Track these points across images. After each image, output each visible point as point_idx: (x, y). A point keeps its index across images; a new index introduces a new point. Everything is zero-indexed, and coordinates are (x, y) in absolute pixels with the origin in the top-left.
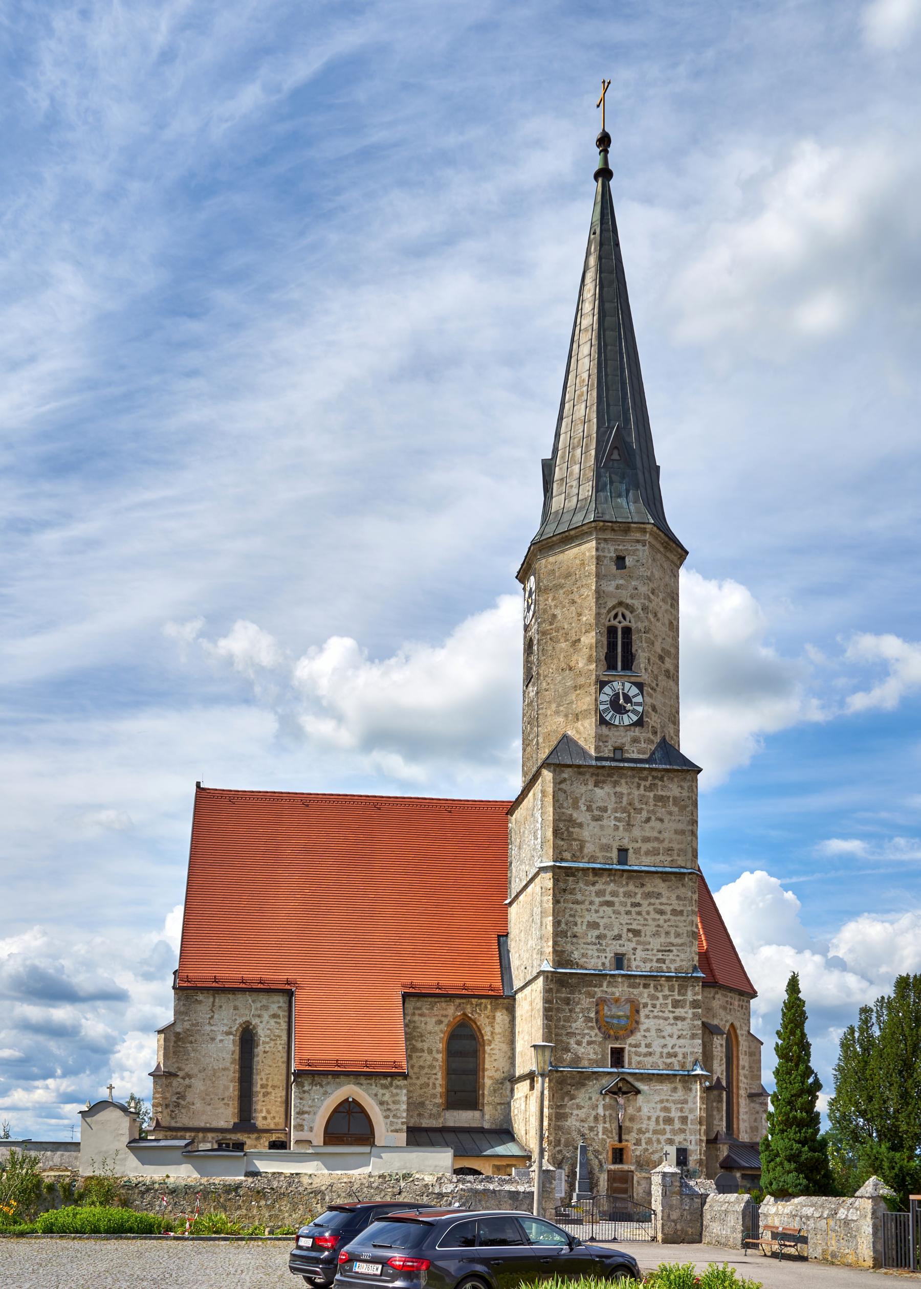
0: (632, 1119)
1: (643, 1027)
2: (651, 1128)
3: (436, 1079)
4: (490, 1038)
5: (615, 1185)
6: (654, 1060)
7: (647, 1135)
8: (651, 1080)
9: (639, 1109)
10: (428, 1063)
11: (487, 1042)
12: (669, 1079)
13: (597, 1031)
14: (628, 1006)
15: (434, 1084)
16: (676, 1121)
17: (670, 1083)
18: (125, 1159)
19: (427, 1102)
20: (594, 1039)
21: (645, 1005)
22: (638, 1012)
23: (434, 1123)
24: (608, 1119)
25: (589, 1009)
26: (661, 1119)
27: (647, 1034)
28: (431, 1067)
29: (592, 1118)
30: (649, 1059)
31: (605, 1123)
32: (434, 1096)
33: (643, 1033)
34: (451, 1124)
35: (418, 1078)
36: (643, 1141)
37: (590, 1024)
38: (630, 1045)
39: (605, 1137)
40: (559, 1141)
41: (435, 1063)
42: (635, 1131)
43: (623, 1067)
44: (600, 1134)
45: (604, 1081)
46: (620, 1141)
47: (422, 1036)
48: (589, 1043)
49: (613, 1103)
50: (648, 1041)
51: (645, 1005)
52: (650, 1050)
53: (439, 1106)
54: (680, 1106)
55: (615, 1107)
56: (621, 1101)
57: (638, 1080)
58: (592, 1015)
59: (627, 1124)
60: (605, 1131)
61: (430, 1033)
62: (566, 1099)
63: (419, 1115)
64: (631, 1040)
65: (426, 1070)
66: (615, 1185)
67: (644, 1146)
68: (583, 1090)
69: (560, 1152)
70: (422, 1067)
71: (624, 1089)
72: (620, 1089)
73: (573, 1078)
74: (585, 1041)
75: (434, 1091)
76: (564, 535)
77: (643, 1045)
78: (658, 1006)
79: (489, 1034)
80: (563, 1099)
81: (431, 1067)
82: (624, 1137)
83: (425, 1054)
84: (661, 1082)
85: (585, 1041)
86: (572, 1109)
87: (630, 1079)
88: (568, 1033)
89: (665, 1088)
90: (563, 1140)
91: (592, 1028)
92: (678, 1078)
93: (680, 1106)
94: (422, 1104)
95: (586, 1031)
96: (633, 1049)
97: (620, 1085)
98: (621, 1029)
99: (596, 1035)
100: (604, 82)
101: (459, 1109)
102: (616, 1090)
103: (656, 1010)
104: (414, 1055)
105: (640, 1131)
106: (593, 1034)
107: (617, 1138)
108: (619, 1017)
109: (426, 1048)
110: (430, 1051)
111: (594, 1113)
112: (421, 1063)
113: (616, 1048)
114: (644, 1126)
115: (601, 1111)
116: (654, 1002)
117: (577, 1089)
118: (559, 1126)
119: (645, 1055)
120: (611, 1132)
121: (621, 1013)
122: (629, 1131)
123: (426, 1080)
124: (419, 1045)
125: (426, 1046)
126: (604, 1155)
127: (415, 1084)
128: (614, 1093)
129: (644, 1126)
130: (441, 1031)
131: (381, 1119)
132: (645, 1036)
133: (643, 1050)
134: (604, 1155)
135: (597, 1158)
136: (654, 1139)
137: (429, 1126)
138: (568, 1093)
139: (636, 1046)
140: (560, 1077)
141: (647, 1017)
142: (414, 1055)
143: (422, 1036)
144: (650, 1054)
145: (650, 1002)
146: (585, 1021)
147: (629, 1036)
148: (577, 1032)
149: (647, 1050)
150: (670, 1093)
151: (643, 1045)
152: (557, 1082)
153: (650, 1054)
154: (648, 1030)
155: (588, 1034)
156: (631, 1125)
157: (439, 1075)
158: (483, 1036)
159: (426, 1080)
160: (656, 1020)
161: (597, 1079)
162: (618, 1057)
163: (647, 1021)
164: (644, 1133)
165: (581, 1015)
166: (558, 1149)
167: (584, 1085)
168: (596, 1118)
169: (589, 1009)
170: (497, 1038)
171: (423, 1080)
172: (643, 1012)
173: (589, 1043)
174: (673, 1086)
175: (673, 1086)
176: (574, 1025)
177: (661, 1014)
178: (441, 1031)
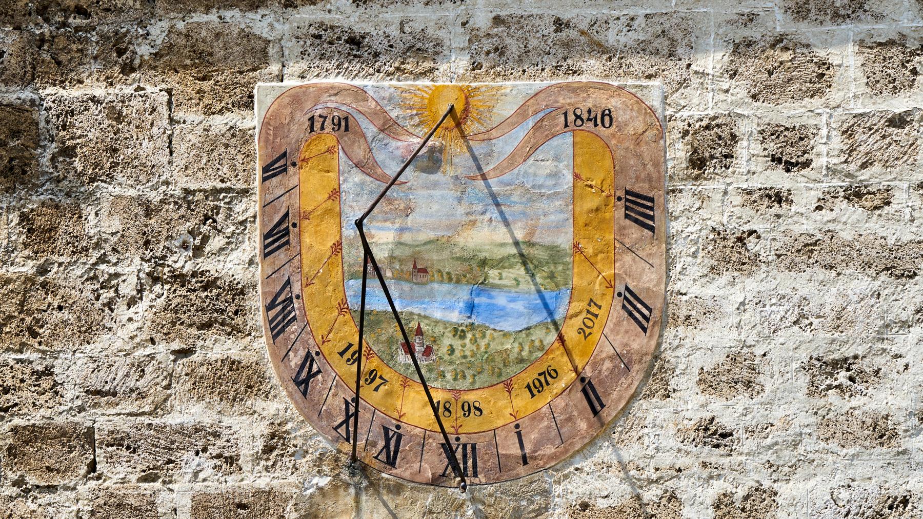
1: (694, 348)
13: (279, 404)
18: (392, 258)
21: (711, 150)
22: (641, 208)
25: (205, 211)
33: (691, 403)
37: (218, 348)
51: (711, 150)
58: (237, 261)
78: (826, 151)
88: (32, 435)
91: (236, 383)
95: (189, 412)
99: (275, 443)
100: (347, 129)
103: (804, 188)
106: (246, 430)
108: (475, 271)
116: (790, 112)
132: (715, 435)
141: (734, 251)
145: (752, 116)
146: (171, 320)
148: (105, 420)
154: (738, 374)
155: (202, 437)
160: (804, 284)
163: (730, 291)
165: (132, 269)
169: (205, 211)
172: (698, 212)
176: (74, 367)
177: (850, 220)
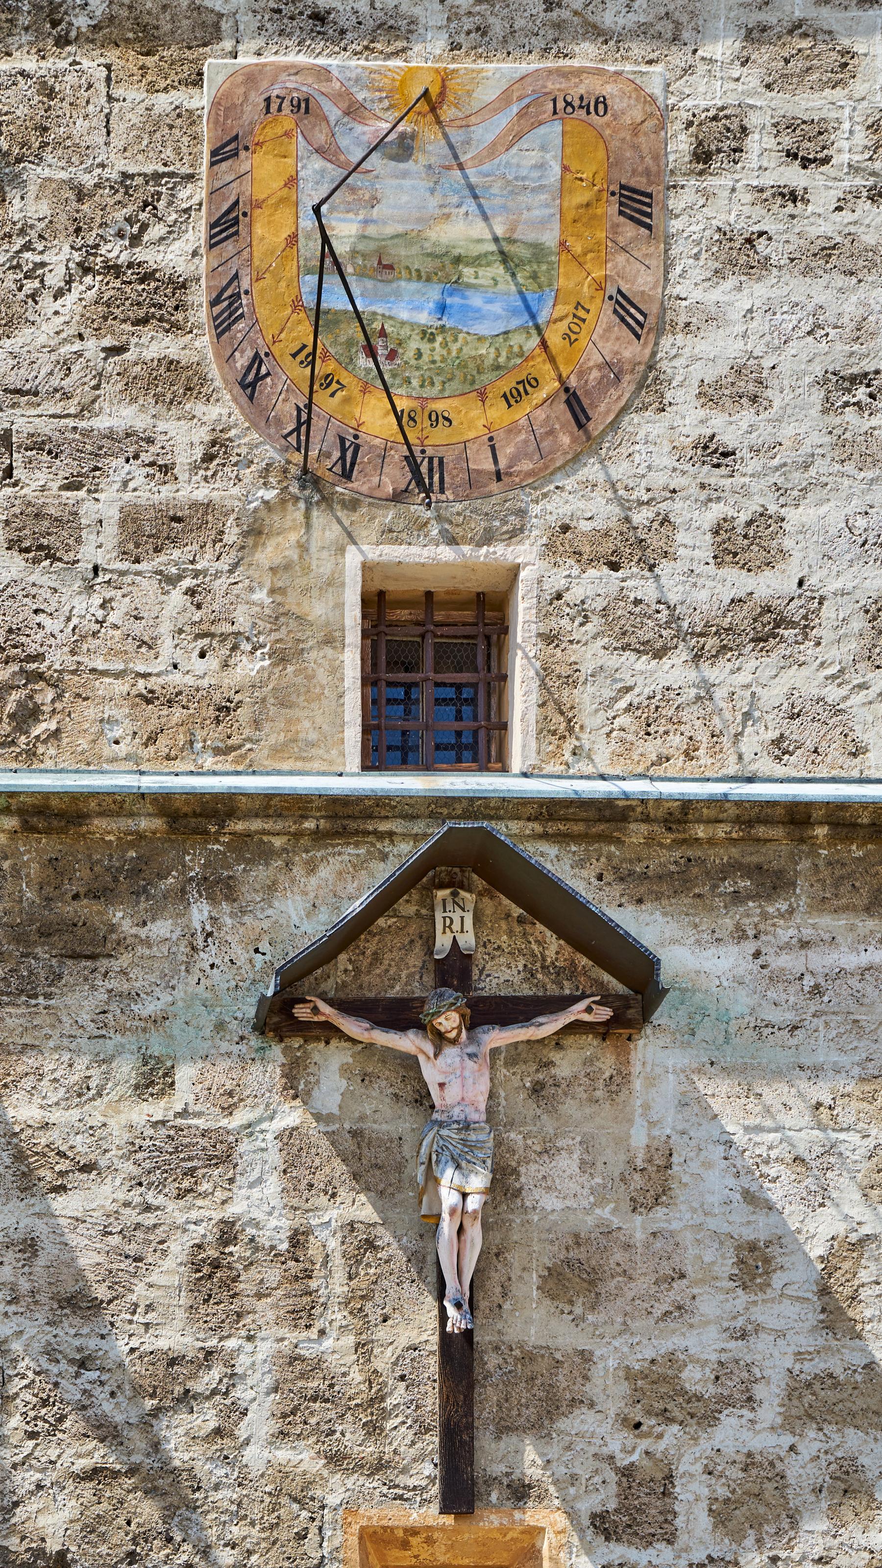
1: (693, 359)
6: (806, 681)
7: (731, 1434)
8: (773, 883)
9: (654, 1181)
13: (223, 409)
14: (542, 153)
20: (190, 490)
22: (637, 204)
25: (146, 197)
27: (732, 428)
29: (169, 1271)
30: (765, 679)
31: (303, 1314)
33: (689, 419)
36: (693, 1496)
37: (154, 345)
38: (562, 539)
43: (504, 770)
44: (258, 1423)
48: (150, 533)
49: (386, 1117)
50: (747, 494)
52: (770, 585)
56: (459, 1078)
57: (644, 886)
58: (179, 252)
59: (530, 1322)
60: (305, 1397)
64: (580, 500)
71: (500, 977)
74: (105, 505)
76: (299, 765)
77: (693, 543)
82: (492, 1455)
85: (105, 505)
87: (568, 868)
91: (175, 384)
95: (118, 415)
96: (592, 584)
98: (473, 381)
99: (215, 451)
103: (822, 187)
105: (659, 1395)
106: (183, 435)
108: (447, 269)
111: (190, 1222)
113: (484, 768)
114: (701, 1344)
116: (809, 103)
119: (716, 640)
120: (374, 1414)
121: (463, 231)
122: (549, 1403)
133: (694, 583)
136: (801, 1471)
139: (631, 547)
141: (741, 254)
144: (769, 627)
145: (765, 109)
147: (546, 472)
149: (734, 582)
151: (693, 543)
153: (769, 627)
154: (744, 387)
155: (133, 443)
160: (821, 291)
161: (219, 887)
162: (435, 664)
163: (737, 297)
165: (60, 258)
167: (89, 948)
168: (213, 1273)
169: (146, 197)
172: (699, 211)
173: (150, 533)
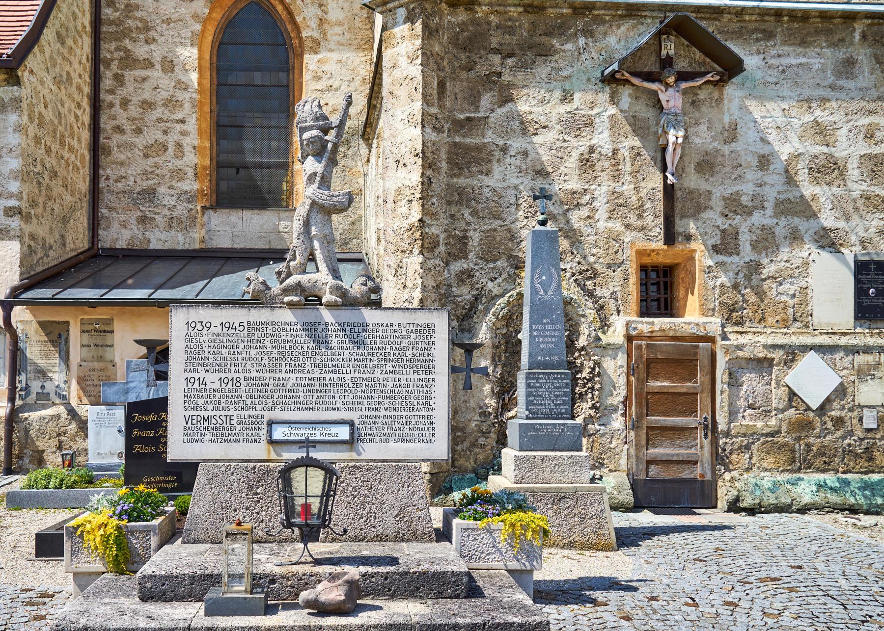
0: (707, 165)
2: (771, 194)
3: (184, 133)
4: (316, 35)
5: (655, 384)
7: (757, 218)
8: (769, 35)
10: (164, 94)
11: (308, 44)
12: (829, 32)
15: (179, 145)
16: (853, 172)
17: (832, 45)
19: (162, 190)
23: (178, 240)
24: (627, 167)
26: (802, 166)
28: (171, 103)
29: (572, 162)
32: (179, 175)
34: (223, 242)
35: (139, 131)
36: (745, 239)
39: (617, 226)
40: (463, 240)
41: (180, 95)
42: (717, 203)
45: (612, 40)
46: (670, 238)
47: (147, 29)
49: (646, 112)
53: (191, 198)
54: (865, 121)
55: (647, 127)
56: (672, 98)
60: (617, 204)
61: (168, 21)
62: (486, 100)
63: (143, 220)
65: (159, 112)
66: (655, 384)
67: (747, 253)
68: (542, 71)
69: (465, 276)
70: (147, 105)
72: (667, 63)
73: (511, 31)
75: (179, 163)
79: (314, 24)
80: (474, 100)
81: (171, 103)
82: (680, 225)
83: (156, 74)
84: (803, 43)
86: (507, 133)
89: (816, 63)
90: (475, 238)
92: (859, 27)
93: (865, 121)
94: (150, 194)
97: (669, 48)
101: (252, 209)
102: (650, 65)
104: (129, 75)
105: (734, 206)
107: (658, 231)
109: (157, 57)
110: (169, 65)
111: (579, 146)
112: (147, 95)
114: (747, 188)
115: (602, 139)
117: (522, 66)
118: (461, 191)
122: (698, 205)
123: (159, 136)
124: (140, 51)
125: (157, 53)
126: (615, 285)
127: (131, 146)
128: (650, 77)
129: (747, 188)
130: (195, 17)
131: (524, 385)
134: (615, 285)
135: (590, 294)
137: (167, 246)
138: (492, 80)
140: (463, 26)
142: (129, 75)
143: (147, 29)
150: (831, 79)
152: (454, 41)
156: (703, 186)
157: (192, 125)
158: (299, 31)
159: (159, 136)
161: (588, 33)
164: (748, 212)
166: (458, 266)
167: (545, 53)
170: (333, 33)
171: (153, 135)
174: (841, 54)
175: (841, 54)
178: (195, 17)
